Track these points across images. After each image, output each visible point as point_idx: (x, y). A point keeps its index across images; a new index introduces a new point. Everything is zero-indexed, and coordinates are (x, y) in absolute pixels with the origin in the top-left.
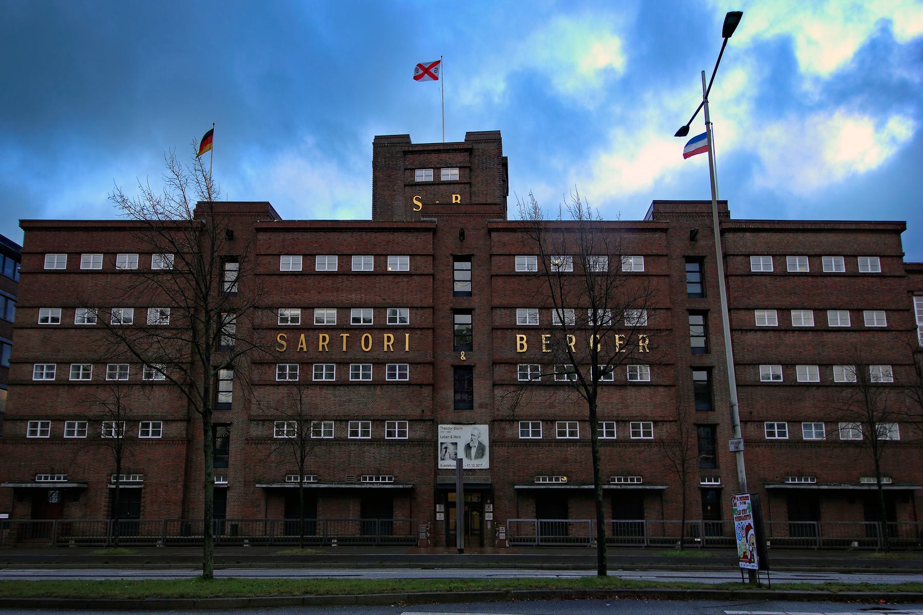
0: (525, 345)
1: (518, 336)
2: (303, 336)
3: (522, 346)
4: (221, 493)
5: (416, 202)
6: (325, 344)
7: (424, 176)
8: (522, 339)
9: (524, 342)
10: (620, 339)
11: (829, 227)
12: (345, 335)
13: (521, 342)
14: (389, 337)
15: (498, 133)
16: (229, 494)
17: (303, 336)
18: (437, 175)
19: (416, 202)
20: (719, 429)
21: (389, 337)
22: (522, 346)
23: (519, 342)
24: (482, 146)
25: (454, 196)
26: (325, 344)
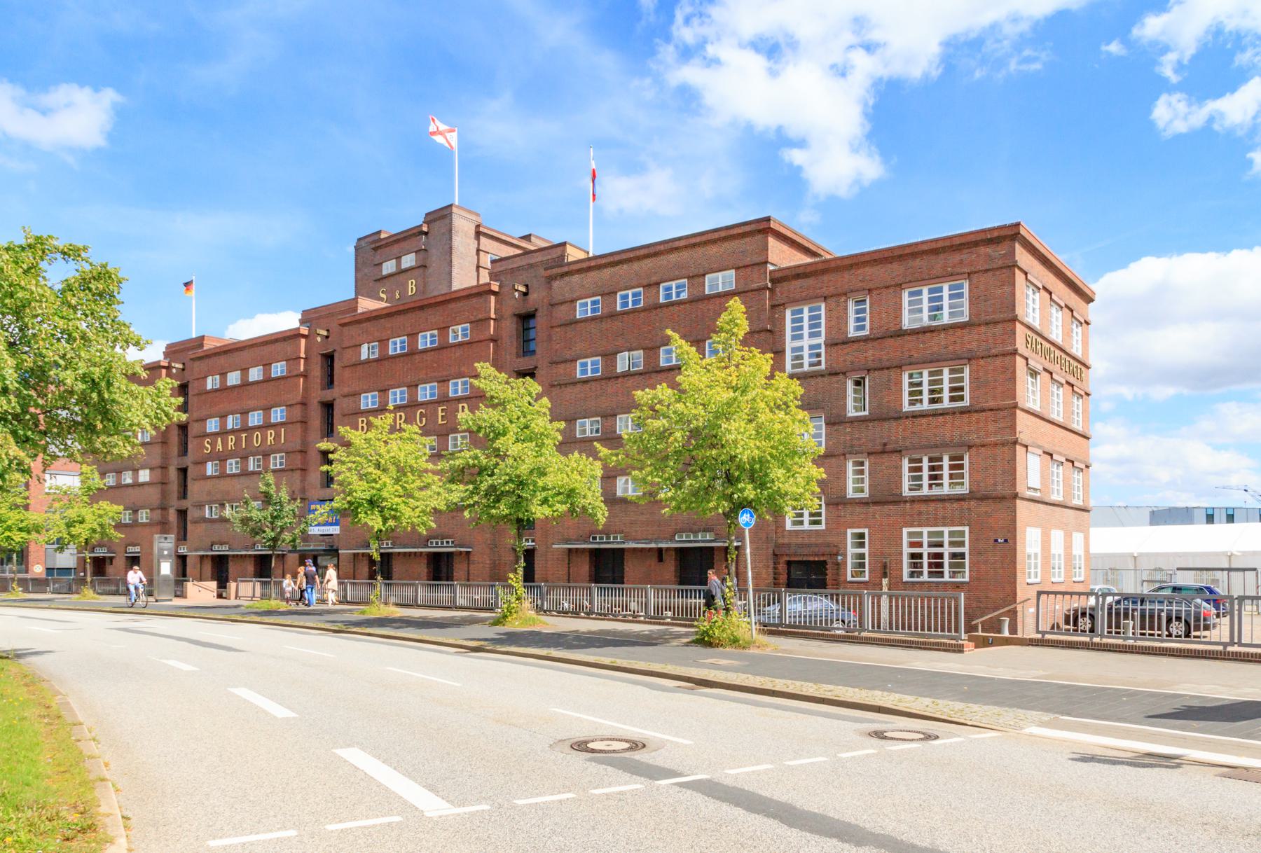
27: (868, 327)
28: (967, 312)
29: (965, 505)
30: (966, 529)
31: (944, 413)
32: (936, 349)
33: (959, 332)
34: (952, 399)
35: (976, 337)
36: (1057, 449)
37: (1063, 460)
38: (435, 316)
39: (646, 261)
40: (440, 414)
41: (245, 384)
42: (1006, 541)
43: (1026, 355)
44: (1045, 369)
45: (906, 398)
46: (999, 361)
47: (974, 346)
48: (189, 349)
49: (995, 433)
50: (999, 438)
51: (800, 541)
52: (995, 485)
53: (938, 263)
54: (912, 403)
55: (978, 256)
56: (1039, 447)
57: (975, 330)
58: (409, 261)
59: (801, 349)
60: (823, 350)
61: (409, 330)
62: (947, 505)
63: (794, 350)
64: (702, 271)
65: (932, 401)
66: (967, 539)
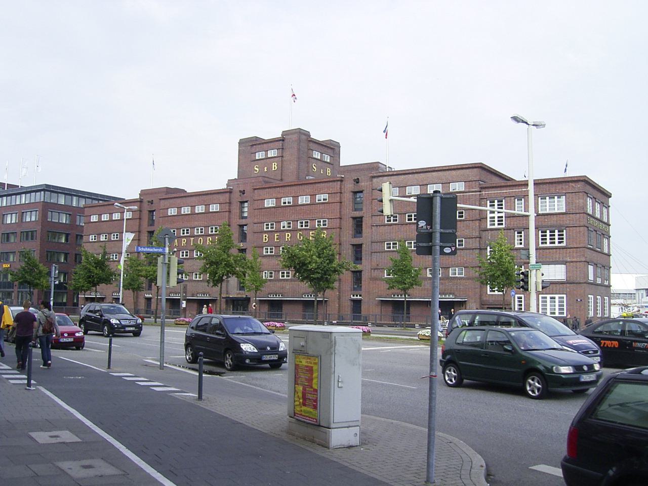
0: (267, 239)
1: (287, 234)
2: (176, 240)
3: (266, 239)
4: (149, 299)
5: (257, 169)
6: (289, 237)
7: (260, 155)
8: (266, 236)
9: (267, 238)
10: (277, 236)
11: (432, 170)
12: (192, 239)
13: (265, 237)
14: (288, 235)
15: (154, 226)
16: (152, 300)
17: (176, 240)
18: (179, 211)
19: (256, 169)
20: (363, 273)
21: (288, 235)
22: (266, 239)
23: (264, 238)
24: (289, 137)
25: (273, 164)
26: (289, 237)
27: (458, 213)
28: (564, 209)
29: (565, 285)
30: (565, 296)
31: (556, 248)
32: (552, 222)
33: (561, 216)
34: (499, 224)
35: (569, 218)
36: (599, 262)
37: (601, 266)
38: (309, 189)
39: (421, 174)
40: (276, 237)
41: (179, 215)
42: (581, 300)
43: (588, 226)
44: (594, 230)
45: (489, 223)
46: (578, 228)
47: (568, 222)
48: (159, 193)
49: (577, 257)
50: (578, 259)
51: (494, 299)
52: (577, 278)
53: (553, 188)
54: (491, 225)
55: (569, 186)
56: (592, 262)
57: (568, 216)
58: (272, 153)
59: (494, 218)
60: (504, 219)
61: (294, 195)
62: (557, 285)
63: (491, 218)
64: (449, 182)
65: (559, 243)
66: (458, 215)
